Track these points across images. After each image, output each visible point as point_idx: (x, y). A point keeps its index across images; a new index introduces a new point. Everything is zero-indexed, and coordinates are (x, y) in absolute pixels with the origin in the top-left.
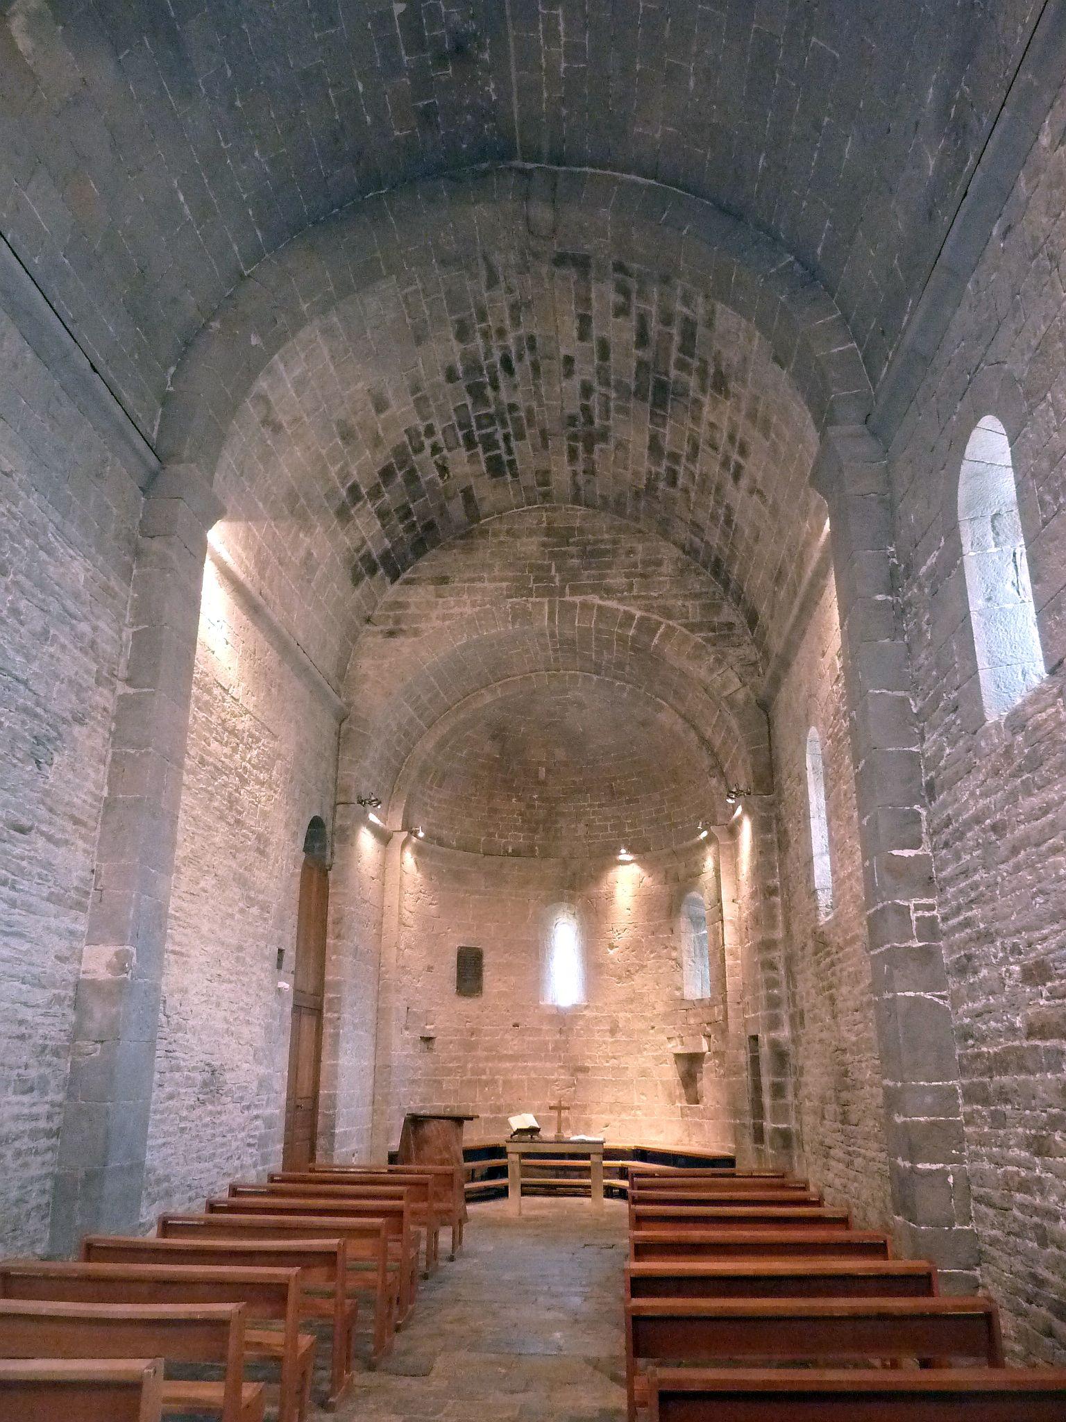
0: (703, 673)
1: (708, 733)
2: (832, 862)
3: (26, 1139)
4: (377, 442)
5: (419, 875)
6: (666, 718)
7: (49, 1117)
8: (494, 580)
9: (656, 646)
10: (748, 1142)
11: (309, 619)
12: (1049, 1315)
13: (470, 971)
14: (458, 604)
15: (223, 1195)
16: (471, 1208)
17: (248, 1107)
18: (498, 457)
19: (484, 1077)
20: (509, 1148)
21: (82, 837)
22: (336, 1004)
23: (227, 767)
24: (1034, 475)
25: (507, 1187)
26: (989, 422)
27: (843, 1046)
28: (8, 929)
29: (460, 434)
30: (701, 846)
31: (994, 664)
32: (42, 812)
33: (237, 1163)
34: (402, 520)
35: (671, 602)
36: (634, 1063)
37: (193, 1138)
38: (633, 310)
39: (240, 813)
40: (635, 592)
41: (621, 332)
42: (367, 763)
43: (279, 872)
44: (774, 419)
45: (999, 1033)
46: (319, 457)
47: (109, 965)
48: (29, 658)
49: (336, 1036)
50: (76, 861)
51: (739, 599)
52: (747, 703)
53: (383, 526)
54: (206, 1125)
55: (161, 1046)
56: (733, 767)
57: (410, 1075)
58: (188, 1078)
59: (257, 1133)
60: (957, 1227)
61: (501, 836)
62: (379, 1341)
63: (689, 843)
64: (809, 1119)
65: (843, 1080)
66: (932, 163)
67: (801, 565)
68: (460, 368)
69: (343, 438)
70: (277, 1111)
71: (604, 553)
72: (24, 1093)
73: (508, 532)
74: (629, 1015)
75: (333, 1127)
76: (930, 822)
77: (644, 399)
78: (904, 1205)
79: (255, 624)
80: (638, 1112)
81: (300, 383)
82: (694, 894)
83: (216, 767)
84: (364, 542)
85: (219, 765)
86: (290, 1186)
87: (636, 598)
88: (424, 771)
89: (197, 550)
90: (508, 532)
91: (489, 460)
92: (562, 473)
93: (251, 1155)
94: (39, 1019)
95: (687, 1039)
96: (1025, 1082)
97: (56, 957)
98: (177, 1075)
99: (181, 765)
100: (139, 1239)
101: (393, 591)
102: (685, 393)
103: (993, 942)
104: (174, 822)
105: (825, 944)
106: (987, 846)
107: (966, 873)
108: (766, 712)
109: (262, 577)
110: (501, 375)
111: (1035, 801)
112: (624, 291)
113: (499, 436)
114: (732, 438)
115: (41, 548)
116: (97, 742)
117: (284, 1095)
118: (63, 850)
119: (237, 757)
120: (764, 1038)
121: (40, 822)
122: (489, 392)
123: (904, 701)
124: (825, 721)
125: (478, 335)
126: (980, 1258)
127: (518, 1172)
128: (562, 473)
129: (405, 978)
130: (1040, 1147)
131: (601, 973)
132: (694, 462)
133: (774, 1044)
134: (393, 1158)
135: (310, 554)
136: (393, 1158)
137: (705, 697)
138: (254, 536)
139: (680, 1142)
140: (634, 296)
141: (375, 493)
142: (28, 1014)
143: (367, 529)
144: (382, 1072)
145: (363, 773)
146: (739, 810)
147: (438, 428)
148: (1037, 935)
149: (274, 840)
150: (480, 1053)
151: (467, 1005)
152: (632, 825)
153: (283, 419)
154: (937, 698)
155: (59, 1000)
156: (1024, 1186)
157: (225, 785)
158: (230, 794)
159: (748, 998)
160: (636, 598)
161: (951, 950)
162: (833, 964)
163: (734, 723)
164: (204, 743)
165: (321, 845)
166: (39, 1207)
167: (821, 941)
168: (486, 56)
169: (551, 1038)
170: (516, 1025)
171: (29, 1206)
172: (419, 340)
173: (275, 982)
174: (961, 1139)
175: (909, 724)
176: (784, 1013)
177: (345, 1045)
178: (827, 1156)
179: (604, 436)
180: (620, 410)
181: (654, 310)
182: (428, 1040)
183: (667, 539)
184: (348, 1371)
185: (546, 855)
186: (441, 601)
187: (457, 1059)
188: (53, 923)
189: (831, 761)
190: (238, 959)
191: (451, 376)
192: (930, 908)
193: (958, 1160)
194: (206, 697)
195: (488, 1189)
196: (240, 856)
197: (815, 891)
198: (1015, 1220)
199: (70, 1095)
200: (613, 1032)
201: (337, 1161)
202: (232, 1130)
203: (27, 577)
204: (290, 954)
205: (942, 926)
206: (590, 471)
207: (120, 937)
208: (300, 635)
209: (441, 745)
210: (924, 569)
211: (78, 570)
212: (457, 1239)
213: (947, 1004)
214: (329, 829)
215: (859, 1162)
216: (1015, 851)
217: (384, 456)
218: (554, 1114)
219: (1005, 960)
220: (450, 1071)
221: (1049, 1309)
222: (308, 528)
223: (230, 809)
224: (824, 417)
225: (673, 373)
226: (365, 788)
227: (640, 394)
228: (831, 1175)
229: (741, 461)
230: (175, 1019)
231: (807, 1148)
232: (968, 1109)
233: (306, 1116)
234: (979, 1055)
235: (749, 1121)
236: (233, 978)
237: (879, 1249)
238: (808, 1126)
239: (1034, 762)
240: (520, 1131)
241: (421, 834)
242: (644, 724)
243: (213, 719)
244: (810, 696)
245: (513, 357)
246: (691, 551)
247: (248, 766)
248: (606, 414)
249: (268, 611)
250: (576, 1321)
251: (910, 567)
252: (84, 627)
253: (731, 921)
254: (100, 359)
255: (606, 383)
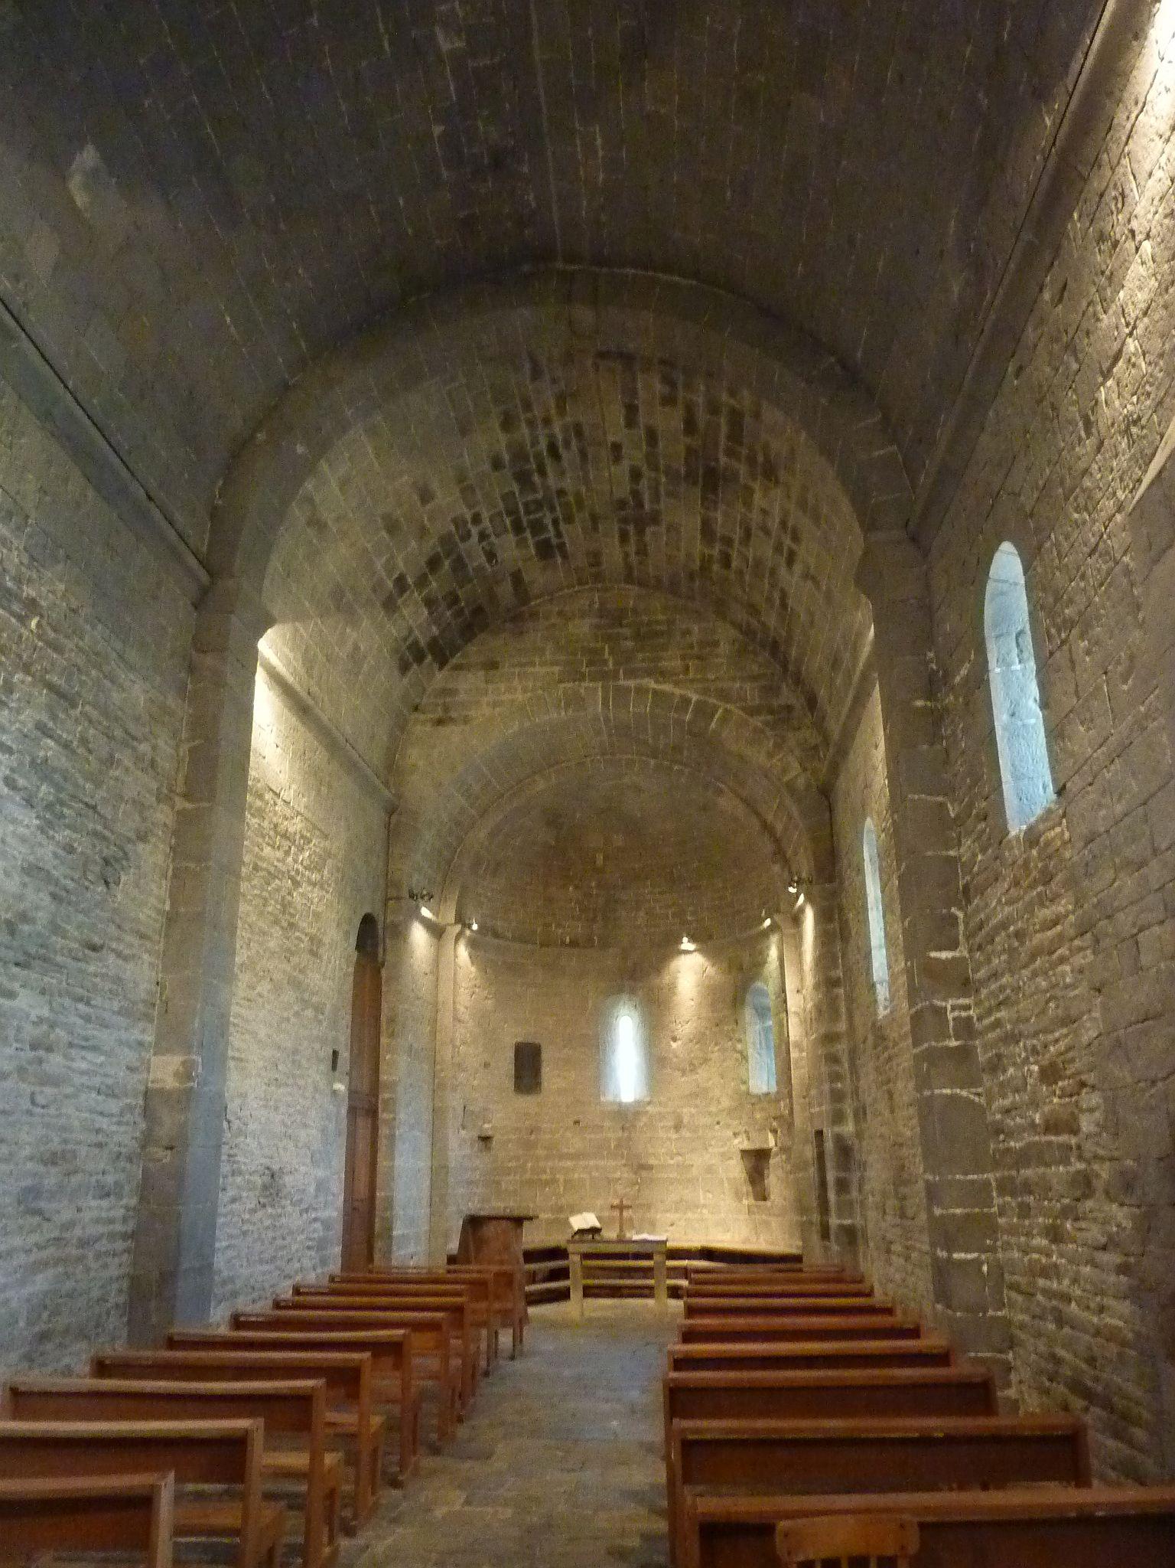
0: (762, 759)
1: (770, 818)
2: (888, 956)
3: (104, 1241)
4: (423, 532)
5: (473, 969)
6: (727, 803)
7: (125, 1220)
8: (543, 664)
9: (714, 731)
10: (815, 1238)
11: (354, 713)
12: (1066, 1391)
13: (527, 1066)
14: (509, 690)
15: (287, 1295)
16: (532, 1310)
17: (307, 1211)
18: (547, 541)
19: (544, 1177)
20: (571, 1248)
21: (147, 951)
22: (390, 1104)
23: (280, 871)
24: (1042, 608)
25: (568, 1289)
26: (1007, 547)
27: (900, 1140)
28: (84, 1043)
29: (508, 522)
30: (766, 934)
31: (1017, 777)
32: (112, 929)
33: (297, 1265)
34: (449, 607)
35: (725, 685)
36: (698, 1161)
37: (255, 1241)
38: (680, 400)
39: (292, 916)
40: (691, 675)
41: (668, 422)
42: (418, 857)
43: (332, 971)
44: (825, 510)
45: (1022, 1129)
46: (365, 550)
47: (176, 1074)
48: (98, 784)
49: (392, 1137)
50: (142, 973)
51: (798, 680)
52: (808, 786)
53: (431, 613)
54: (268, 1228)
55: (225, 1149)
56: (796, 854)
57: (468, 1175)
58: (249, 1182)
59: (316, 1235)
60: (991, 1313)
61: (559, 925)
62: (443, 1434)
63: (754, 931)
64: (872, 1215)
65: (901, 1178)
66: (956, 289)
67: (855, 658)
68: (506, 457)
69: (389, 532)
70: (335, 1214)
71: (658, 634)
72: (101, 1198)
73: (560, 613)
74: (693, 1110)
75: (390, 1229)
76: (966, 924)
77: (695, 483)
78: (943, 1294)
79: (304, 723)
80: (705, 1211)
81: (344, 483)
82: (759, 984)
83: (269, 873)
84: (411, 631)
85: (272, 869)
86: (349, 1286)
87: (692, 681)
88: (476, 864)
89: (249, 659)
90: (560, 613)
91: (538, 545)
92: (613, 554)
93: (311, 1258)
94: (114, 1128)
95: (753, 1135)
96: (1043, 1177)
97: (128, 1068)
98: (239, 1179)
99: (238, 876)
100: (209, 1332)
101: (440, 678)
102: (735, 476)
103: (1017, 1042)
104: (233, 934)
105: (884, 1038)
106: (1012, 952)
107: (995, 975)
108: (827, 797)
109: (310, 676)
110: (549, 463)
111: (1045, 913)
112: (668, 381)
113: (548, 521)
114: (783, 524)
115: (106, 677)
116: (160, 859)
117: (341, 1198)
118: (130, 966)
119: (290, 859)
120: (828, 1133)
121: (111, 939)
122: (536, 478)
123: (942, 806)
124: (879, 814)
125: (523, 425)
126: (1012, 1343)
127: (579, 1273)
128: (613, 554)
129: (462, 1076)
130: (1055, 1235)
131: (664, 1067)
132: (747, 545)
133: (839, 1139)
134: (452, 1260)
135: (356, 648)
136: (452, 1260)
137: (765, 782)
138: (302, 636)
139: (746, 1240)
140: (680, 387)
141: (422, 582)
142: (103, 1123)
143: (414, 618)
144: (439, 1172)
145: (416, 868)
146: (802, 898)
147: (485, 515)
148: (1050, 1037)
149: (326, 940)
150: (541, 1152)
151: (526, 1103)
152: (693, 913)
153: (328, 517)
154: (971, 805)
155: (130, 1108)
156: (1046, 1272)
157: (278, 890)
158: (283, 898)
159: (813, 1092)
160: (692, 681)
161: (986, 1047)
162: (890, 1059)
163: (795, 811)
164: (260, 850)
165: (373, 942)
166: (117, 1305)
167: (880, 1035)
168: (526, 169)
169: (613, 1135)
170: (577, 1122)
171: (109, 1305)
172: (464, 431)
173: (330, 1084)
174: (993, 1230)
175: (944, 829)
176: (848, 1108)
177: (402, 1147)
178: (888, 1251)
179: (655, 518)
180: (669, 494)
181: (701, 400)
182: (486, 1139)
183: (724, 619)
184: (414, 1453)
185: (605, 945)
186: (491, 687)
187: (517, 1158)
188: (124, 1035)
189: (883, 855)
190: (294, 1062)
191: (497, 464)
192: (967, 1008)
193: (993, 1249)
194: (259, 803)
195: (549, 1291)
196: (295, 960)
197: (873, 985)
198: (1039, 1304)
199: (143, 1199)
200: (677, 1127)
201: (394, 1263)
202: (291, 1233)
203: (94, 706)
204: (345, 1055)
205: (978, 1026)
206: (642, 551)
207: (188, 1049)
208: (348, 729)
209: (492, 835)
210: (958, 679)
211: (136, 693)
212: (518, 1339)
213: (983, 1100)
214: (380, 926)
215: (914, 1255)
216: (1033, 957)
217: (431, 545)
218: (616, 1213)
219: (1026, 1061)
220: (508, 1171)
221: (1066, 1385)
222: (355, 623)
223: (284, 913)
224: (869, 522)
225: (723, 459)
226: (417, 881)
227: (690, 477)
228: (892, 1270)
229: (794, 547)
230: (236, 1124)
231: (871, 1244)
232: (1001, 1201)
233: (365, 1219)
234: (1008, 1150)
235: (816, 1217)
236: (290, 1081)
237: (915, 1333)
238: (875, 1222)
239: (1047, 878)
240: (581, 1232)
241: (475, 927)
242: (705, 808)
243: (266, 824)
244: (866, 787)
245: (560, 444)
246: (748, 632)
247: (300, 868)
248: (656, 498)
249: (317, 710)
250: (633, 1412)
251: (948, 675)
252: (144, 748)
253: (796, 1013)
254: (152, 484)
255: (656, 469)
